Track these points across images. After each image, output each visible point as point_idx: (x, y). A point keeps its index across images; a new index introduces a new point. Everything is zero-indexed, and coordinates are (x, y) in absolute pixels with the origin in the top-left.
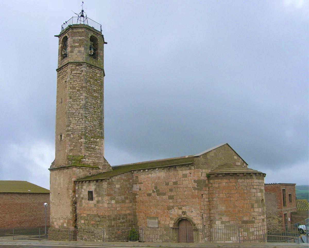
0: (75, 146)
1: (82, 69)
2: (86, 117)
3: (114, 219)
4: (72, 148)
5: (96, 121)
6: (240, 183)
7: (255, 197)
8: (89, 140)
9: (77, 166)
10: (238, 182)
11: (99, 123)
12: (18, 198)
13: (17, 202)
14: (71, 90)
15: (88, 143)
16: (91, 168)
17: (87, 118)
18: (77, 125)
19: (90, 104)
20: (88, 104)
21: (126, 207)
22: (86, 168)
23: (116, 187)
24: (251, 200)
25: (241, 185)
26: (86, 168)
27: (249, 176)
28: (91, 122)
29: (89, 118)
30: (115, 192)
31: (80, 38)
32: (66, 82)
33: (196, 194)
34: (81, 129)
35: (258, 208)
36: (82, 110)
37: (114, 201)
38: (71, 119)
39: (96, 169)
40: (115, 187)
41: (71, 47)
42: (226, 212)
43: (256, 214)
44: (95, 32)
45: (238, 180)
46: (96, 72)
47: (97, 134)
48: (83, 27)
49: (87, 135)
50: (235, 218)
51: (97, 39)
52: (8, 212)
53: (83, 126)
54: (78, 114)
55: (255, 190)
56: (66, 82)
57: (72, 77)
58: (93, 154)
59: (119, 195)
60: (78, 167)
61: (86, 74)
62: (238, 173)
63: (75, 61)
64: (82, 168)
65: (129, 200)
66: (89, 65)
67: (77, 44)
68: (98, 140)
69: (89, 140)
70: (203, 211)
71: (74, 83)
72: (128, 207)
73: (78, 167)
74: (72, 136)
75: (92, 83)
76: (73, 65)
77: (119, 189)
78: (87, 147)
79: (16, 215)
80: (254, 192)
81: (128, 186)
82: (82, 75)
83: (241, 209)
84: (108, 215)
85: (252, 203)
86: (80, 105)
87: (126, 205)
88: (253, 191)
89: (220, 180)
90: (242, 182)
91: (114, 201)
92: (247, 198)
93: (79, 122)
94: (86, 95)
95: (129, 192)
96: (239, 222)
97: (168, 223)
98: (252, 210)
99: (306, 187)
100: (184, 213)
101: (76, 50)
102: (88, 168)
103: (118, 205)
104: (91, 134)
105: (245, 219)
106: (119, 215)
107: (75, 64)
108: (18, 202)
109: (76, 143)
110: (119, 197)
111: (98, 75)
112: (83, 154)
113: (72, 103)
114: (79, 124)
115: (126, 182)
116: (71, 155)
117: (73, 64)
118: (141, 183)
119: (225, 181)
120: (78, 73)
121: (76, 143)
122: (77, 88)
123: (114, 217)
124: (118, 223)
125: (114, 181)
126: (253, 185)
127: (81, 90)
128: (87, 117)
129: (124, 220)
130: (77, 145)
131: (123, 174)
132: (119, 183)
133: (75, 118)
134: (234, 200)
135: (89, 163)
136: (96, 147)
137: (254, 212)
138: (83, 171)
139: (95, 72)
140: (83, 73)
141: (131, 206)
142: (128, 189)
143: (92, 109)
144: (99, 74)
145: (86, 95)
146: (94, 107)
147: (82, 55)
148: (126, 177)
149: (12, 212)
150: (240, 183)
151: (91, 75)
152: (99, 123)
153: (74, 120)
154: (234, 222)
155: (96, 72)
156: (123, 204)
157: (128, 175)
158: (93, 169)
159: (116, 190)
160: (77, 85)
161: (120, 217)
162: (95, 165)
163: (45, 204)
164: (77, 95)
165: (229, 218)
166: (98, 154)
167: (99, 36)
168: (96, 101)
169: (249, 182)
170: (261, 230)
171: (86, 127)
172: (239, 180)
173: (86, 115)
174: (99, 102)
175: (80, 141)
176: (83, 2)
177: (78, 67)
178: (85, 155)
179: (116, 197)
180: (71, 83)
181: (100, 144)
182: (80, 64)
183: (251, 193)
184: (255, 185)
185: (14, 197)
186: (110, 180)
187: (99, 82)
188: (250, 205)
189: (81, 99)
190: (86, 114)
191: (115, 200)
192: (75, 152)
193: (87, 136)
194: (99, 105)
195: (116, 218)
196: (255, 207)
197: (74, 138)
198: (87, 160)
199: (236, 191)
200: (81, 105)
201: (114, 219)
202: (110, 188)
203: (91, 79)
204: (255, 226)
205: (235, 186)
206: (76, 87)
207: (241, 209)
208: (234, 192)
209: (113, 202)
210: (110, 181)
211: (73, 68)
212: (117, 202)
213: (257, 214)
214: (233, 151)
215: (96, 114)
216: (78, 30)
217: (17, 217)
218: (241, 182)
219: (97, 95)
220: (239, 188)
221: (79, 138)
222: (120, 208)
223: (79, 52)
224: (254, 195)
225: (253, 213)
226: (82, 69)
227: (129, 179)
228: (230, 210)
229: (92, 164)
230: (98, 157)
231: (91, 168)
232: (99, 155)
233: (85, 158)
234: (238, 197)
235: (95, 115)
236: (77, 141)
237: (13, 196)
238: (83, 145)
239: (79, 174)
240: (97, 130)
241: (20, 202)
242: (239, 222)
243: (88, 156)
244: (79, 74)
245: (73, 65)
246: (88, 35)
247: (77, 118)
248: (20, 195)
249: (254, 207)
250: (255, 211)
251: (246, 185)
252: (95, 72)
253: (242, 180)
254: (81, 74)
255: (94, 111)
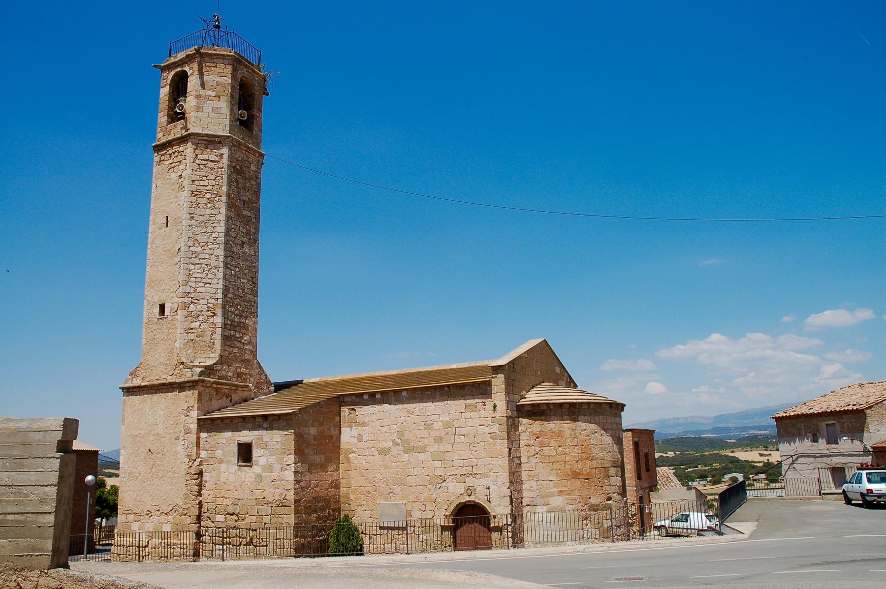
31: (218, 79)
32: (180, 176)
33: (657, 455)
41: (199, 97)
56: (180, 176)
97: (430, 515)
99: (884, 445)
100: (470, 491)
101: (208, 106)
114: (210, 281)
118: (363, 424)
163: (90, 478)
170: (139, 547)
221: (209, 314)
223: (216, 110)
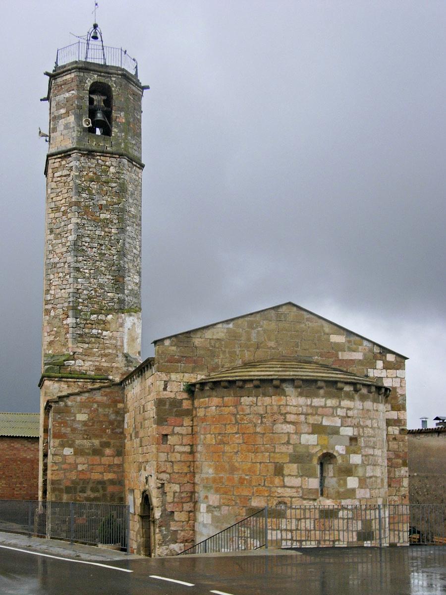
0: (57, 334)
1: (71, 164)
2: (77, 269)
3: (68, 490)
4: (52, 338)
5: (106, 275)
6: (245, 407)
7: (291, 447)
8: (86, 320)
9: (53, 377)
10: (241, 403)
11: (113, 279)
12: (26, 448)
13: (25, 455)
14: (52, 215)
15: (82, 326)
16: (89, 381)
17: (81, 272)
18: (61, 290)
19: (87, 239)
20: (84, 240)
21: (105, 465)
22: (75, 380)
23: (77, 419)
24: (274, 452)
25: (248, 411)
26: (75, 380)
27: (270, 388)
28: (91, 280)
29: (86, 271)
30: (74, 430)
34: (67, 296)
35: (301, 476)
36: (70, 255)
37: (72, 450)
38: (52, 277)
39: (102, 381)
40: (73, 418)
42: (214, 480)
43: (288, 492)
44: (101, 72)
45: (240, 400)
46: (107, 163)
47: (107, 303)
48: (72, 69)
49: (79, 308)
50: (232, 500)
51: (109, 88)
52: (4, 476)
53: (71, 290)
54: (62, 265)
55: (294, 427)
57: (53, 185)
58: (97, 350)
59: (84, 437)
60: (55, 377)
61: (78, 174)
62: (238, 380)
63: (60, 150)
64: (65, 380)
65: (111, 450)
66: (85, 152)
67: (63, 111)
68: (110, 317)
69: (86, 320)
70: (165, 476)
71: (59, 198)
72: (109, 465)
73: (56, 379)
74: (52, 313)
75: (94, 192)
76: (55, 159)
77: (85, 423)
78: (81, 335)
79: (21, 483)
80: (285, 432)
81: (113, 417)
82: (71, 178)
83: (247, 477)
84: (54, 478)
85: (276, 461)
86: (67, 245)
87: (105, 460)
88: (282, 429)
89: (207, 399)
90: (251, 403)
91: (72, 450)
92: (263, 448)
93: (65, 282)
94: (79, 221)
95: (114, 432)
96: (241, 511)
98: (277, 480)
102: (82, 380)
103: (81, 459)
104: (90, 305)
105: (256, 503)
106: (83, 482)
107: (59, 156)
108: (26, 457)
109: (59, 327)
110: (85, 441)
111: (112, 170)
112: (70, 350)
113: (54, 242)
114: (64, 286)
115: (107, 410)
116: (50, 354)
117: (55, 157)
119: (216, 401)
120: (63, 174)
121: (59, 327)
122: (63, 209)
123: (69, 484)
124: (78, 499)
125: (72, 406)
126: (283, 411)
127: (68, 210)
128: (81, 270)
129: (96, 494)
130: (60, 331)
131: (98, 391)
132: (84, 410)
133: (59, 273)
134: (230, 451)
135: (84, 368)
136: (103, 334)
137: (284, 486)
138: (68, 387)
139: (102, 165)
140: (72, 174)
141: (119, 463)
142: (111, 423)
143: (94, 250)
144: (115, 167)
145: (79, 221)
146: (101, 245)
147: (72, 132)
148: (105, 398)
149: (11, 476)
150: (245, 407)
151: (91, 174)
152: (113, 279)
153: (57, 279)
154: (229, 509)
155: (107, 163)
156: (97, 458)
157: (111, 392)
158: (93, 382)
159: (79, 426)
160: (62, 202)
161: (85, 487)
162: (100, 373)
164: (63, 224)
165: (220, 498)
166: (108, 348)
167: (114, 79)
168: (107, 230)
169: (271, 405)
171: (77, 292)
172: (243, 399)
173: (78, 265)
174: (113, 231)
175: (65, 322)
176: (96, 4)
177: (64, 163)
178: (74, 353)
179: (77, 442)
180: (52, 198)
181: (113, 326)
182: (66, 154)
183: (276, 435)
184: (290, 413)
185: (17, 445)
186: (61, 403)
187: (114, 185)
188: (271, 467)
189: (69, 231)
190: (77, 262)
191: (73, 447)
192: (57, 348)
193: (81, 311)
194: (113, 238)
195: (75, 488)
196: (286, 472)
197: (55, 317)
198: (79, 362)
199: (235, 427)
200: (68, 244)
201: (68, 490)
202: (60, 420)
203: (93, 183)
204: (284, 527)
205: (233, 414)
206: (61, 206)
207: (247, 477)
208: (231, 432)
209: (68, 451)
210: (62, 405)
211: (57, 165)
212: (79, 452)
213: (295, 495)
214: (321, 320)
215: (106, 260)
216: (65, 78)
217: (24, 487)
218: (248, 404)
219: (108, 216)
220: (242, 419)
222: (86, 465)
223: (67, 127)
224: (287, 439)
225: (280, 490)
226: (71, 164)
227: (116, 402)
228: (222, 477)
229: (92, 371)
230: (109, 355)
231: (89, 379)
232: (110, 351)
233: (74, 359)
234: (240, 444)
235: (101, 262)
236: (60, 324)
237: (14, 443)
238: (71, 330)
239: (57, 393)
240: (109, 294)
241: (32, 456)
242: (241, 511)
243: (81, 354)
244: (65, 176)
245: (55, 159)
246: (85, 83)
247: (61, 275)
248: (30, 442)
249: (284, 472)
250: (287, 484)
251: (262, 412)
252: (102, 165)
253: (251, 399)
254: (69, 175)
255: (100, 254)
